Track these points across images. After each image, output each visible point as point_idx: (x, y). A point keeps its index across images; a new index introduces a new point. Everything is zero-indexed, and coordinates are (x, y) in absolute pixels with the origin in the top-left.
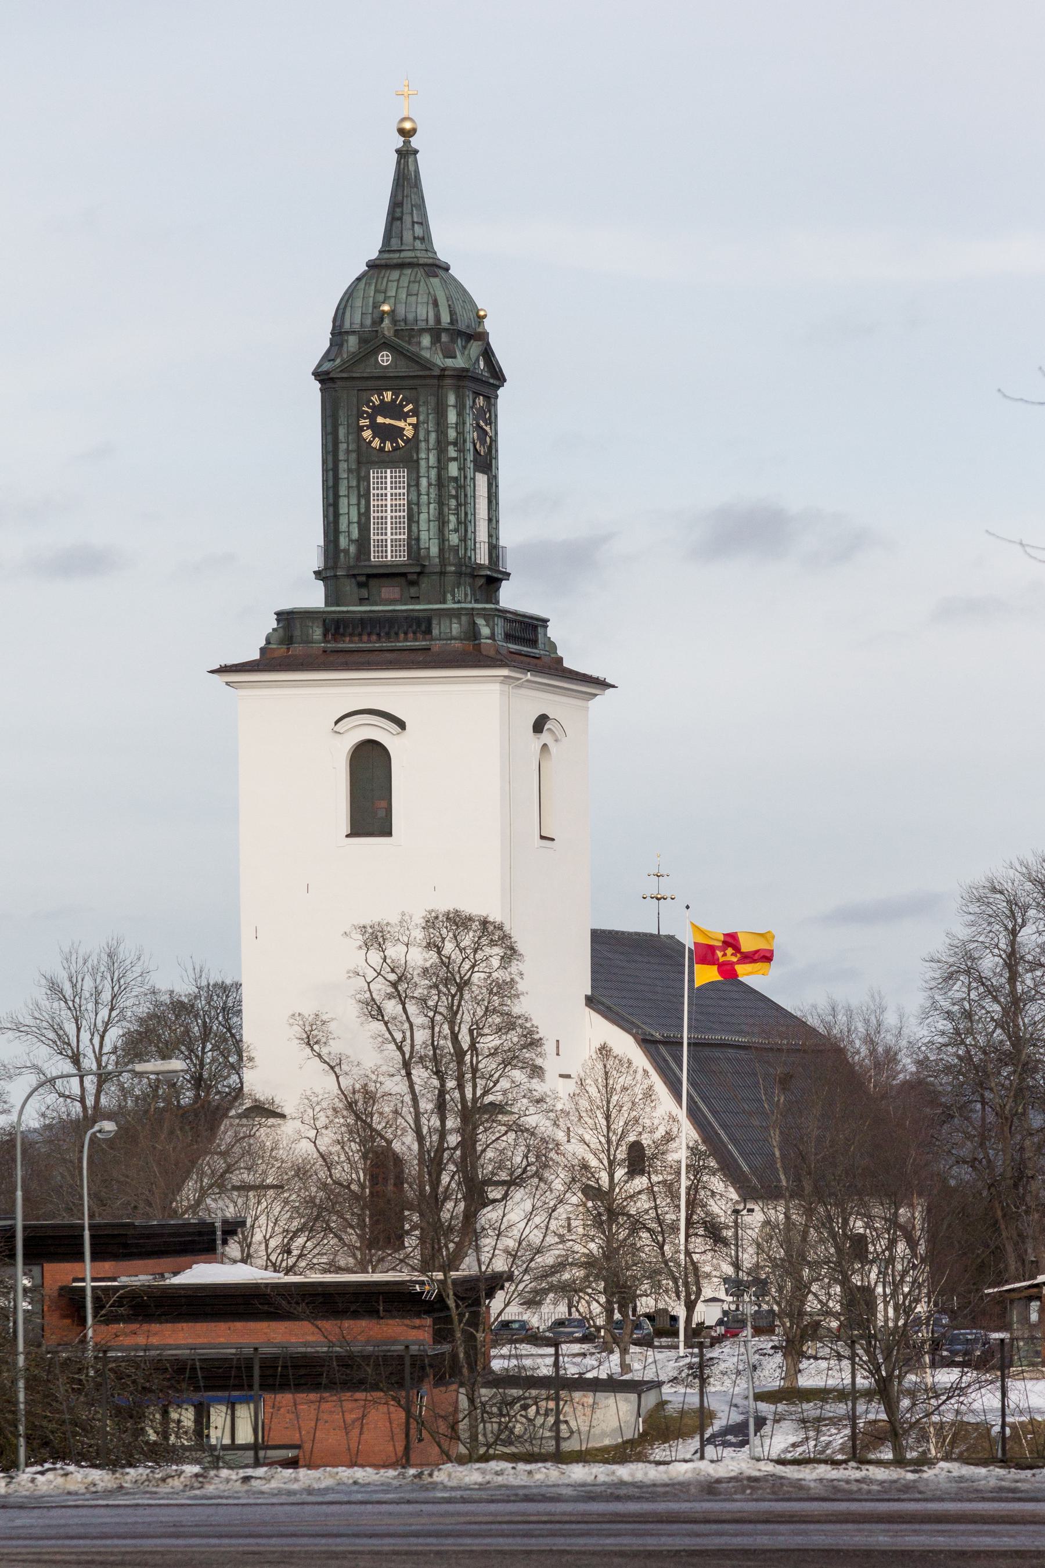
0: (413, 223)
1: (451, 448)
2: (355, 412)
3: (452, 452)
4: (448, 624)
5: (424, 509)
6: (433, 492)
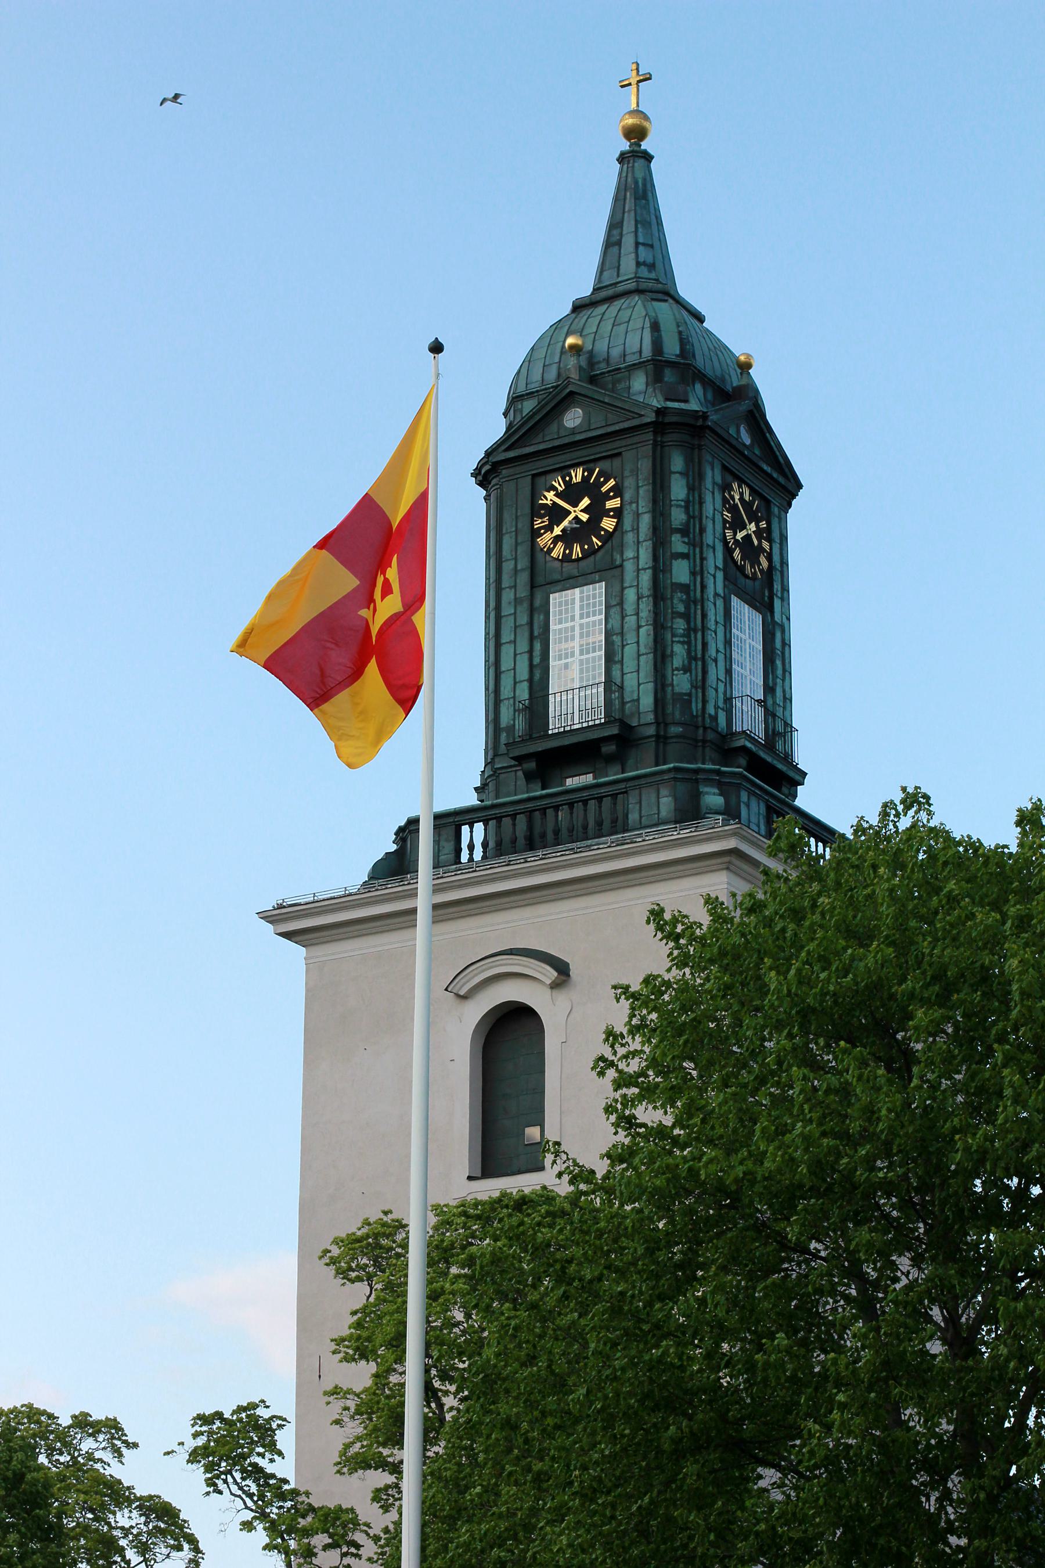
0: (637, 244)
1: (676, 538)
2: (527, 510)
3: (678, 544)
4: (653, 799)
5: (630, 638)
6: (646, 608)
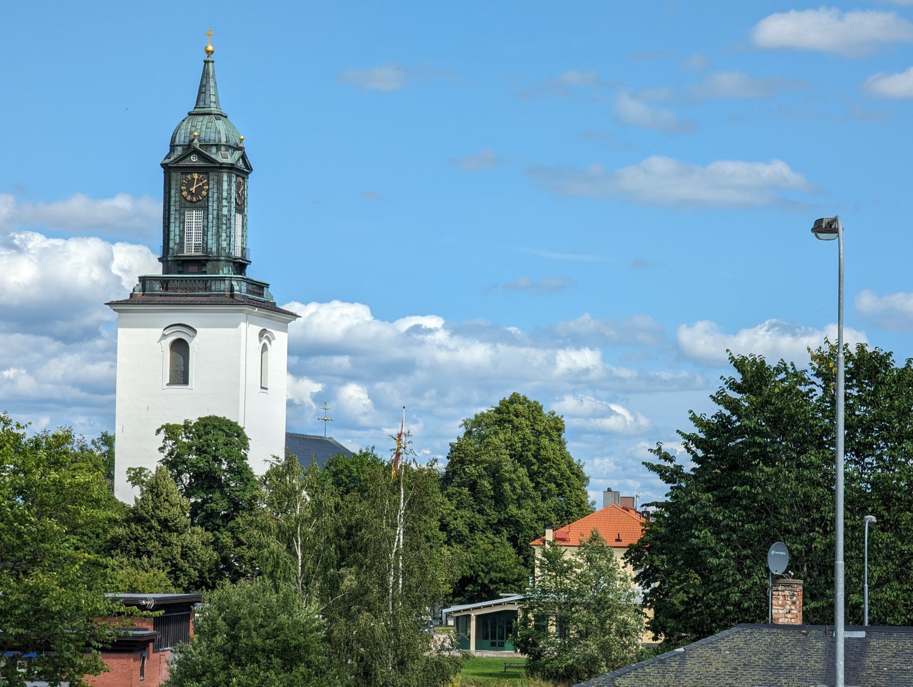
3: (225, 203)
5: (210, 229)
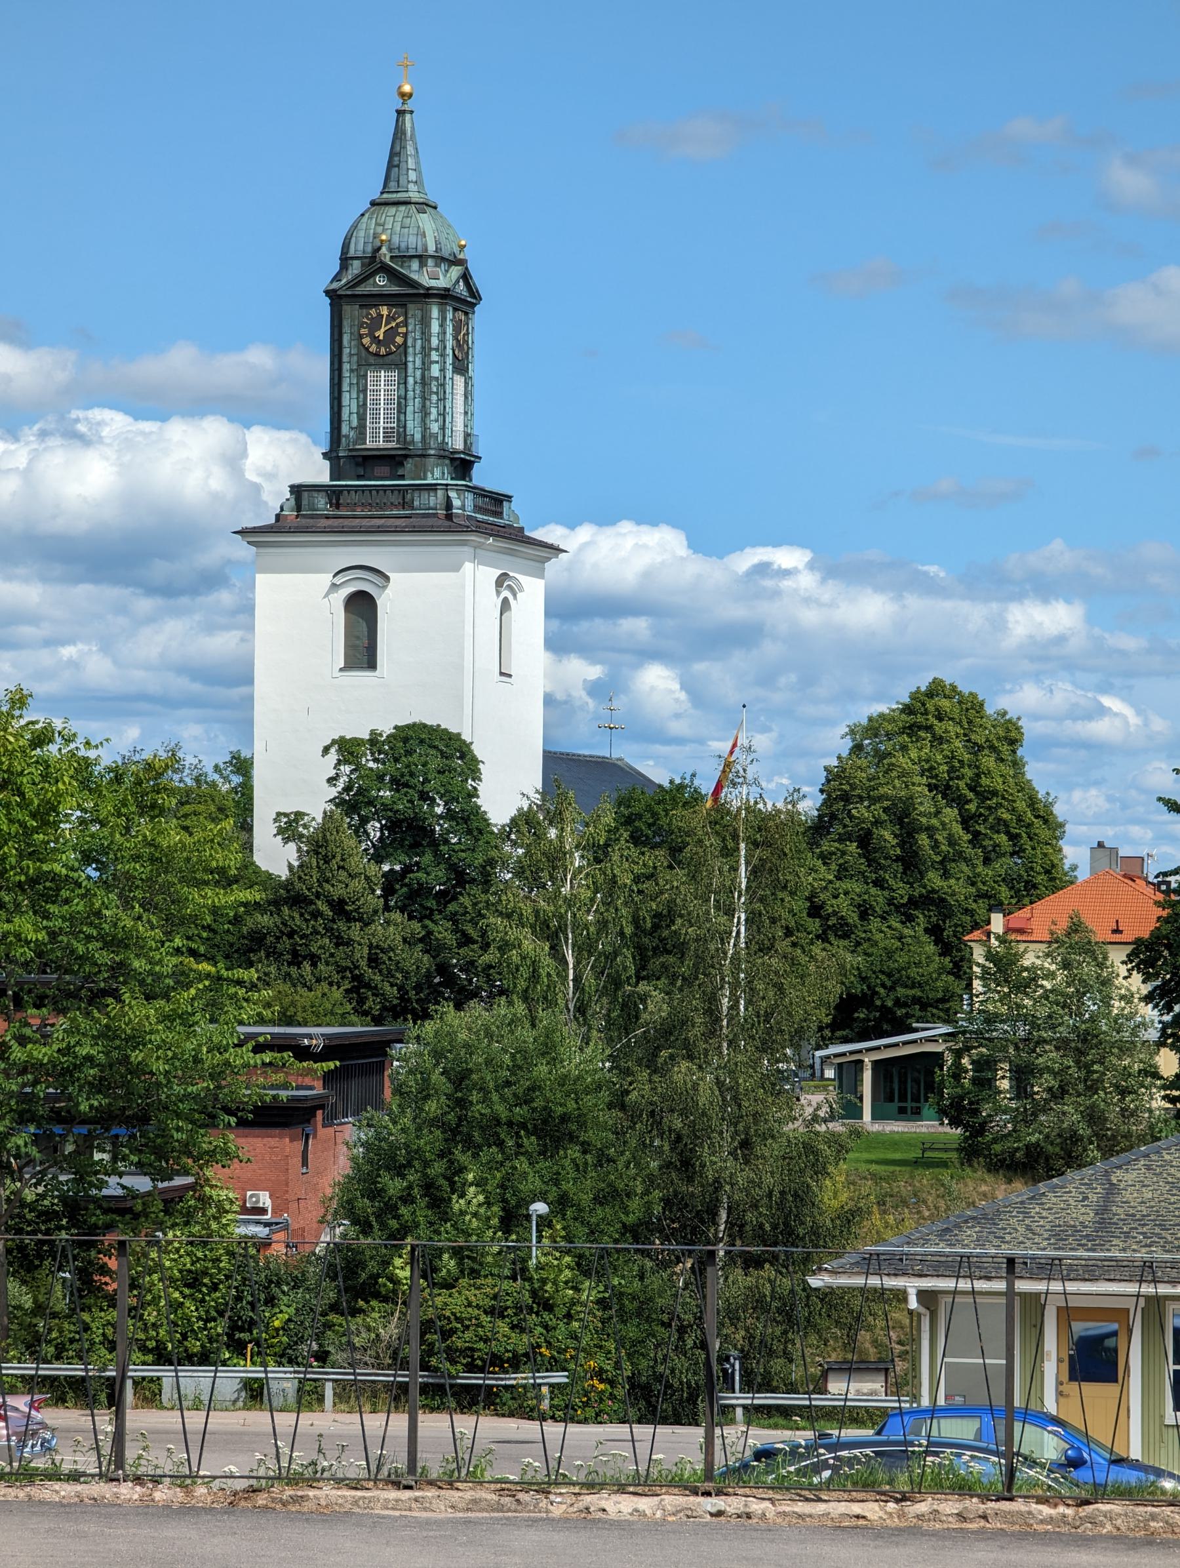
1: (433, 353)
5: (410, 403)
6: (418, 389)
